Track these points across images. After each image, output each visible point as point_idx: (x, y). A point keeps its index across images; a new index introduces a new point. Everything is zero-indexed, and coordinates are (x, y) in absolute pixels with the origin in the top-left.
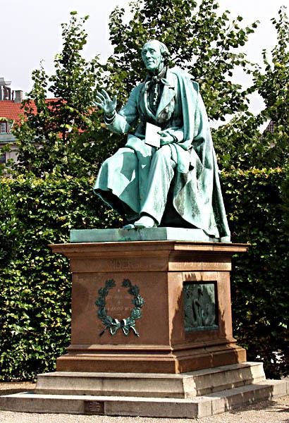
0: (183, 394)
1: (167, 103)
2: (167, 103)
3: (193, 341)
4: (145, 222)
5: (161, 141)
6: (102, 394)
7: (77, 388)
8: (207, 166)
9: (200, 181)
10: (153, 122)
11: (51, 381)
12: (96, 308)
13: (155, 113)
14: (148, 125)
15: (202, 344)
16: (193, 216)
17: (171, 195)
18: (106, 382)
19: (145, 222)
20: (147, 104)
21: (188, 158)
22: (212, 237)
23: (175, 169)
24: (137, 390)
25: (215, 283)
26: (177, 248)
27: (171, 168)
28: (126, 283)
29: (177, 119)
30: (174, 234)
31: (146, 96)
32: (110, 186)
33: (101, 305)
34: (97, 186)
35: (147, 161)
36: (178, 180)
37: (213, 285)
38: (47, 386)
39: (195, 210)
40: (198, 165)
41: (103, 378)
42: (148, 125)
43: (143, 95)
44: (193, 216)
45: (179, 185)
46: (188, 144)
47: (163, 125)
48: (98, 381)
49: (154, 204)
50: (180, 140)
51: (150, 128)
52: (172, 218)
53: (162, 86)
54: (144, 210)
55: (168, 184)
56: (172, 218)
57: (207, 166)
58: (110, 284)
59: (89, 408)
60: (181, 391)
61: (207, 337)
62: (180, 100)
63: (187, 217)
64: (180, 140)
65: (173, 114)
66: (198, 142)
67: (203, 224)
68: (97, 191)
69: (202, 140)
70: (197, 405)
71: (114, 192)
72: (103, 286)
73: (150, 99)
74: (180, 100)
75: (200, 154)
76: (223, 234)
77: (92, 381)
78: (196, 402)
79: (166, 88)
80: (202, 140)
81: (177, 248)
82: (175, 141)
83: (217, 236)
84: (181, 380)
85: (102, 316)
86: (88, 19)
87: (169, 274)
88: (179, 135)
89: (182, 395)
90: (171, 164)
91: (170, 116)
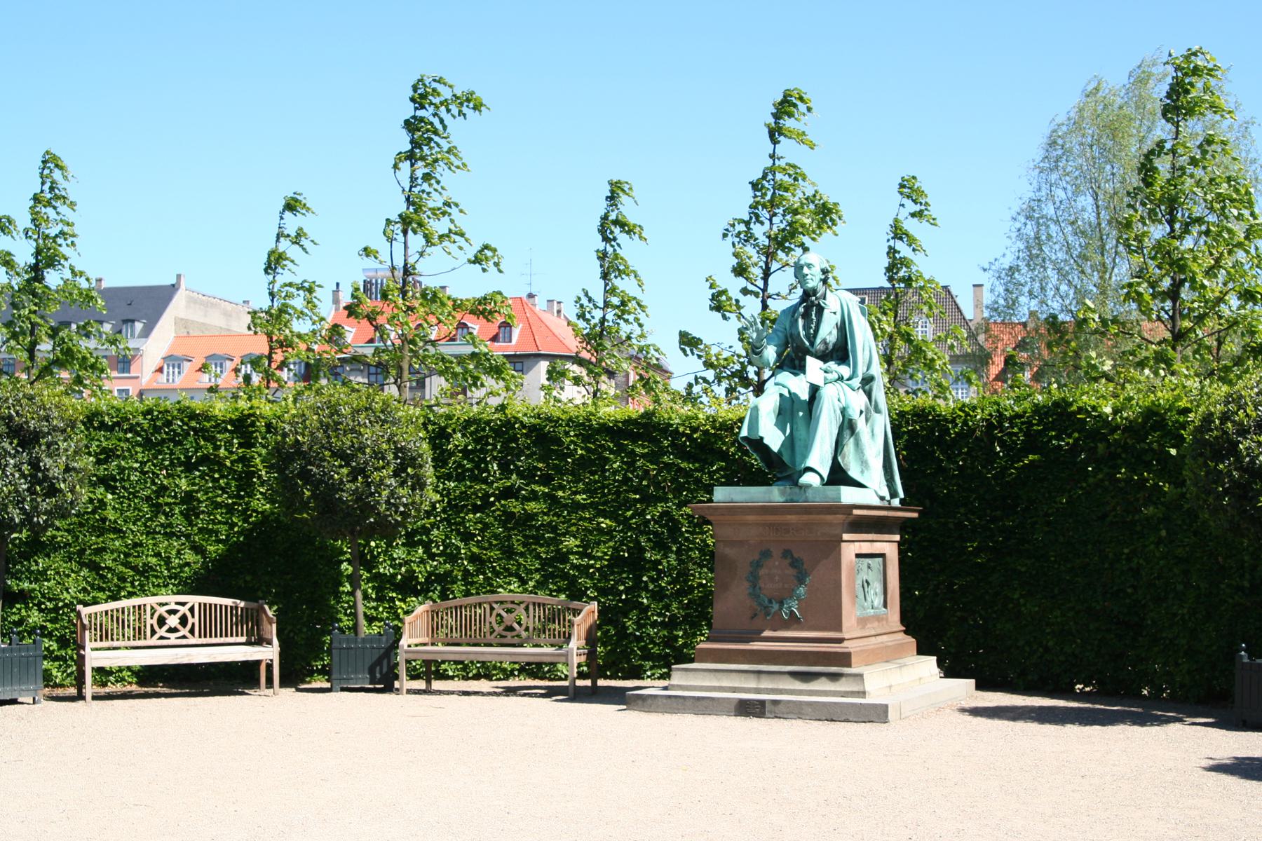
0: (864, 693)
1: (828, 332)
2: (828, 332)
3: (863, 628)
4: (808, 478)
5: (825, 379)
6: (758, 691)
7: (763, 686)
8: (877, 410)
9: (869, 430)
10: (812, 355)
11: (691, 674)
12: (747, 584)
13: (812, 344)
14: (808, 358)
15: (873, 633)
16: (862, 472)
17: (839, 445)
18: (763, 676)
19: (808, 478)
20: (802, 333)
21: (857, 401)
22: (882, 498)
23: (843, 411)
24: (770, 686)
25: (883, 556)
26: (856, 512)
27: (839, 412)
28: (786, 553)
29: (840, 352)
30: (848, 495)
31: (801, 322)
32: (761, 434)
33: (754, 579)
34: (744, 433)
35: (806, 407)
36: (847, 427)
37: (880, 559)
38: (686, 680)
39: (864, 464)
40: (867, 409)
41: (759, 672)
42: (808, 358)
43: (797, 321)
44: (862, 472)
45: (847, 433)
46: (856, 382)
47: (824, 357)
48: (752, 676)
49: (819, 458)
50: (846, 377)
51: (811, 362)
52: (838, 476)
53: (820, 310)
54: (809, 463)
55: (836, 432)
56: (838, 476)
57: (877, 410)
58: (766, 554)
59: (747, 709)
60: (861, 689)
61: (876, 624)
62: (844, 329)
63: (854, 473)
64: (846, 377)
65: (835, 345)
66: (868, 380)
67: (873, 486)
68: (745, 438)
69: (872, 379)
70: (886, 706)
71: (765, 441)
72: (757, 557)
73: (807, 327)
74: (844, 329)
75: (869, 394)
76: (894, 494)
77: (744, 675)
78: (884, 702)
79: (826, 312)
80: (872, 379)
81: (856, 512)
82: (841, 379)
83: (888, 498)
84: (860, 676)
85: (755, 595)
86: (722, 231)
87: (843, 544)
88: (845, 371)
89: (269, 667)
90: (838, 406)
91: (831, 347)
